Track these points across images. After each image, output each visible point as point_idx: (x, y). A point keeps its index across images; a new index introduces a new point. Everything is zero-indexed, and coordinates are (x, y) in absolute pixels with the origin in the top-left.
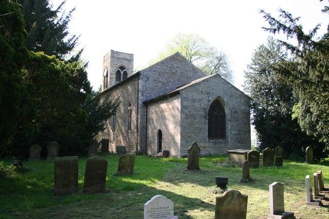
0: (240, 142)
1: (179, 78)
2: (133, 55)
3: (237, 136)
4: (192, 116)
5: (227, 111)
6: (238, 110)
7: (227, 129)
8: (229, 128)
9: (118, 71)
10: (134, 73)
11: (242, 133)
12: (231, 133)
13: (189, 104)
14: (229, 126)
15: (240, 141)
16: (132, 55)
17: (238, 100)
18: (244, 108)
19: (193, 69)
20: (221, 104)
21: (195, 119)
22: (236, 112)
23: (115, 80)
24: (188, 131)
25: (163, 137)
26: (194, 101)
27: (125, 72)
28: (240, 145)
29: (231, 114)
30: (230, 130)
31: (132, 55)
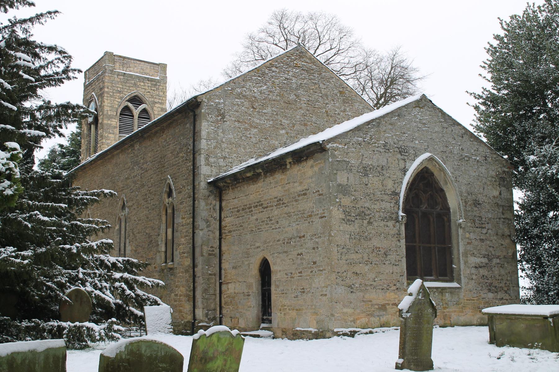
0: (491, 288)
1: (304, 115)
2: (166, 65)
3: (482, 271)
4: (362, 215)
5: (451, 211)
6: (481, 198)
7: (455, 252)
8: (461, 250)
9: (126, 108)
10: (176, 104)
11: (495, 261)
12: (466, 262)
13: (352, 179)
14: (461, 244)
15: (491, 284)
16: (163, 67)
17: (483, 170)
18: (496, 193)
19: (341, 92)
20: (437, 183)
21: (370, 223)
22: (476, 203)
23: (117, 131)
24: (450, 140)
25: (274, 278)
26: (365, 171)
27: (144, 111)
28: (491, 295)
29: (465, 211)
30: (466, 254)
31: (163, 67)
